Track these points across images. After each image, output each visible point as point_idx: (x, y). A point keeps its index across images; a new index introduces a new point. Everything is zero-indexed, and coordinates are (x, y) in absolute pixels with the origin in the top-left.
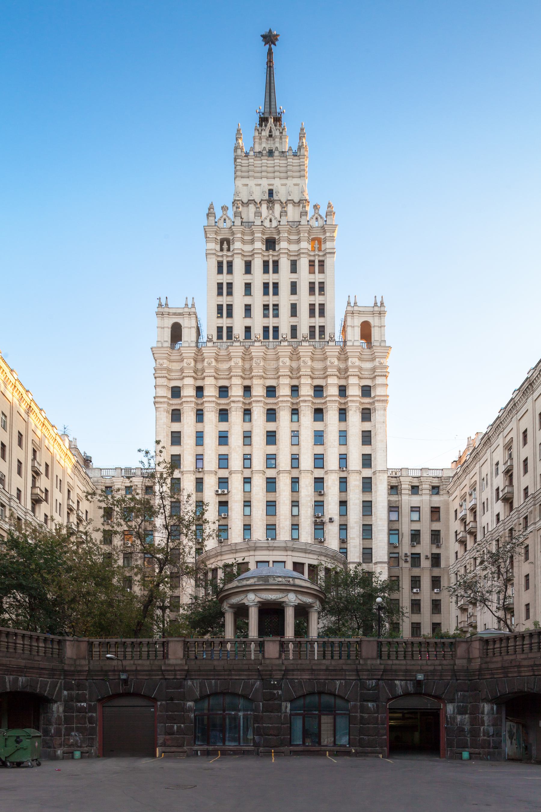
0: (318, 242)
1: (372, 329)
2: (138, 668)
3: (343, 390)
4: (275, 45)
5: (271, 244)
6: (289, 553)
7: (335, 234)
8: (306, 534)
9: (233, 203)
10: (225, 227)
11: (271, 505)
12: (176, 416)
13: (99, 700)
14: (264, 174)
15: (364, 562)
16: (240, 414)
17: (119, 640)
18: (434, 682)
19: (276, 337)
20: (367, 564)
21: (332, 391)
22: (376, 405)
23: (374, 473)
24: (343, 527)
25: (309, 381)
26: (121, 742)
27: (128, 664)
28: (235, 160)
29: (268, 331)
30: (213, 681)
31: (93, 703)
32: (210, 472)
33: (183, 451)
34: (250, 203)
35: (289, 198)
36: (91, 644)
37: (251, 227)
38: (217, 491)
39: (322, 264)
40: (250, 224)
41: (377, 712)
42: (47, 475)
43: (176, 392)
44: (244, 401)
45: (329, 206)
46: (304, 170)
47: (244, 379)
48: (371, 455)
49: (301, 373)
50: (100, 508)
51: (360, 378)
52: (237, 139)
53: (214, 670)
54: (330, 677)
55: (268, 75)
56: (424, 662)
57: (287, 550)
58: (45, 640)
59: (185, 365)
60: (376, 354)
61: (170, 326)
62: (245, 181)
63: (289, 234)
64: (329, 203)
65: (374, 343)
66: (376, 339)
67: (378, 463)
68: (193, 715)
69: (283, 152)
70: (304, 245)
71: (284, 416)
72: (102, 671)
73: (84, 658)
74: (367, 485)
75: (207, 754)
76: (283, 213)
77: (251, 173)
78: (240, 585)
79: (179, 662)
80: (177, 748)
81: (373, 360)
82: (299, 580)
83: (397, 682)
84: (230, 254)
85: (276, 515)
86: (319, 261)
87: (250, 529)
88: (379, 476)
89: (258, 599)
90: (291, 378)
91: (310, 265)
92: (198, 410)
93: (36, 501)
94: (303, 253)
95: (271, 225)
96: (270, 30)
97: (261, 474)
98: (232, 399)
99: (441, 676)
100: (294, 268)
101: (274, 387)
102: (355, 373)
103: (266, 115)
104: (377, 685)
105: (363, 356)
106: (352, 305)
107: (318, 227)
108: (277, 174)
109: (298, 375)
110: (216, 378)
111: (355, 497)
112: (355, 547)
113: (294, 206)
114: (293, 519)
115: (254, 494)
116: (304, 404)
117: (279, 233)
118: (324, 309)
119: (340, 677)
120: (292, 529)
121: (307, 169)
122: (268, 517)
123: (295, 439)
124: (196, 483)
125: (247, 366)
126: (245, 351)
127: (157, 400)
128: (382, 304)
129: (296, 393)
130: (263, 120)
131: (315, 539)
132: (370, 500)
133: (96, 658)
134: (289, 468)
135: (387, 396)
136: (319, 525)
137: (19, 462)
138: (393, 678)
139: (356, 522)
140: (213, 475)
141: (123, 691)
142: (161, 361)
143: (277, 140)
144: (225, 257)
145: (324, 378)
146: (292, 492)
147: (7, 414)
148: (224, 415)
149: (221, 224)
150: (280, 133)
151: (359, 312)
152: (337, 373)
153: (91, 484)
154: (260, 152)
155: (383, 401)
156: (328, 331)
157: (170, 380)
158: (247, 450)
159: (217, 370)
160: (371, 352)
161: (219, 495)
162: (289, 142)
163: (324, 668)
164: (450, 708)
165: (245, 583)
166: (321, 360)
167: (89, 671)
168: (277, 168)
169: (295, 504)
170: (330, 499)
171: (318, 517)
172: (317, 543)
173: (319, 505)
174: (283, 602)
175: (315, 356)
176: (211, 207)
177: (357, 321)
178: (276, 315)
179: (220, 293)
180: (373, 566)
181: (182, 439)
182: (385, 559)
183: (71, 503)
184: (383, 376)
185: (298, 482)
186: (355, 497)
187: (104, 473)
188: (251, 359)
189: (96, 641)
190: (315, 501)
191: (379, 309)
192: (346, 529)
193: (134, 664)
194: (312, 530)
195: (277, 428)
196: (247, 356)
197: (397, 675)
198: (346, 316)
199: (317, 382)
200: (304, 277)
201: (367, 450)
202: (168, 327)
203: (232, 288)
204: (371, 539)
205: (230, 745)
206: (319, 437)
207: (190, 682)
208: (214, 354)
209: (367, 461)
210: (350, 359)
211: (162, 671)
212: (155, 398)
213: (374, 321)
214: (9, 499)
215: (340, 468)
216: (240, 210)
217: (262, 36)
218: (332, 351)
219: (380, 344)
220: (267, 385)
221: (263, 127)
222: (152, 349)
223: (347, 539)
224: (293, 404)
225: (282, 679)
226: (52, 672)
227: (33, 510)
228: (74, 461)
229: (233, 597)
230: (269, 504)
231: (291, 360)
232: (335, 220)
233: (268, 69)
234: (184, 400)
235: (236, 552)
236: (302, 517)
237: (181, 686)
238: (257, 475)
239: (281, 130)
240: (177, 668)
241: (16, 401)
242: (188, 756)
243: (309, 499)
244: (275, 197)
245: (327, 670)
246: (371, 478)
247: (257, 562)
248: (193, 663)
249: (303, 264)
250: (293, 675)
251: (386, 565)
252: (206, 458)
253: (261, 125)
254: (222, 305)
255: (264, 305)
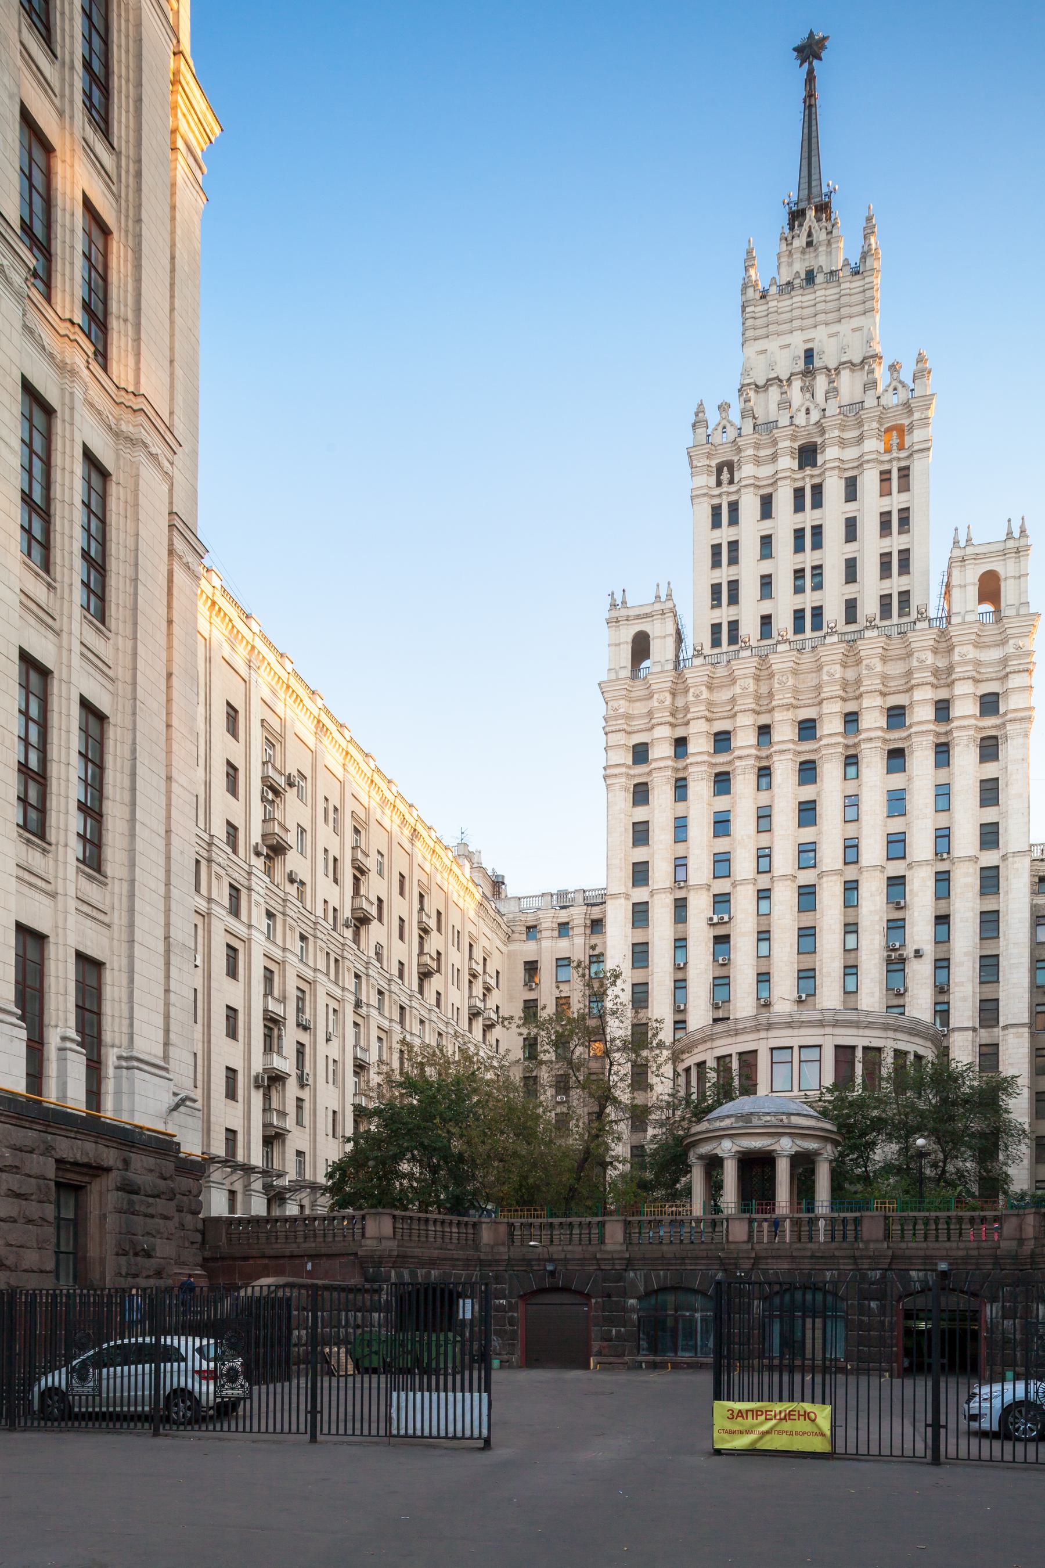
0: (897, 433)
1: (1003, 584)
2: (568, 1256)
3: (943, 709)
4: (820, 59)
5: (808, 455)
6: (828, 1030)
7: (931, 413)
8: (872, 995)
9: (739, 391)
10: (724, 440)
11: (807, 934)
12: (641, 794)
13: (521, 1297)
14: (797, 323)
15: (981, 1026)
16: (752, 778)
17: (544, 1220)
18: (968, 1273)
19: (817, 626)
20: (989, 1030)
21: (922, 714)
22: (1008, 728)
23: (1004, 858)
24: (942, 964)
25: (878, 701)
26: (554, 1349)
27: (555, 1250)
28: (744, 308)
29: (803, 617)
30: (662, 1273)
31: (513, 1301)
32: (699, 887)
33: (653, 855)
34: (771, 385)
35: (843, 360)
36: (511, 1226)
37: (771, 431)
38: (711, 919)
39: (905, 473)
40: (771, 426)
41: (884, 1314)
42: (439, 930)
43: (640, 753)
44: (759, 754)
45: (921, 359)
46: (873, 298)
47: (758, 713)
48: (998, 823)
49: (862, 689)
50: (521, 1034)
51: (976, 681)
52: (746, 269)
53: (663, 1258)
54: (817, 1267)
55: (806, 125)
56: (954, 1245)
57: (824, 1026)
58: (459, 1224)
59: (656, 704)
60: (1009, 632)
61: (630, 639)
62: (761, 345)
63: (843, 431)
64: (920, 354)
65: (1006, 612)
66: (1009, 603)
67: (1011, 839)
68: (635, 1317)
69: (832, 272)
70: (872, 445)
71: (831, 771)
72: (524, 1260)
73: (503, 1244)
74: (990, 880)
75: (654, 1366)
76: (833, 392)
77: (772, 328)
78: (711, 1127)
79: (618, 1248)
80: (616, 1357)
81: (1004, 642)
82: (797, 1118)
83: (913, 1273)
84: (733, 488)
85: (815, 952)
86: (900, 469)
87: (769, 981)
88: (1014, 863)
89: (736, 1148)
90: (844, 700)
91: (882, 481)
92: (677, 780)
93: (425, 975)
94: (868, 461)
95: (808, 419)
96: (811, 34)
97: (789, 882)
98: (737, 753)
99: (977, 1264)
100: (851, 491)
101: (814, 721)
102: (966, 675)
103: (802, 205)
104: (883, 1276)
105: (983, 639)
106: (962, 544)
107: (897, 406)
108: (821, 317)
109: (858, 693)
110: (708, 720)
111: (966, 906)
112: (964, 999)
113: (852, 371)
114: (848, 956)
115: (776, 917)
116: (869, 745)
117: (823, 432)
118: (908, 559)
119: (832, 1267)
120: (845, 975)
121: (878, 295)
122: (801, 956)
123: (851, 813)
124: (676, 907)
125: (764, 690)
126: (759, 664)
127: (609, 772)
128: (1023, 531)
129: (853, 726)
130: (796, 216)
131: (888, 989)
132: (996, 909)
133: (517, 1243)
134: (839, 864)
135: (1031, 708)
136: (896, 963)
137: (401, 920)
138: (907, 1267)
139: (966, 954)
140: (704, 892)
141: (552, 1285)
142: (615, 704)
143: (822, 249)
144: (724, 497)
145: (907, 691)
146: (845, 907)
147: (385, 852)
148: (722, 782)
149: (718, 438)
150: (828, 234)
151: (976, 557)
152: (932, 679)
153: (504, 926)
154: (789, 283)
155: (1022, 719)
156: (915, 601)
157: (630, 733)
158: (764, 840)
159: (710, 704)
160: (999, 628)
161: (714, 924)
162: (845, 250)
163: (809, 1254)
164: (991, 1311)
165: (718, 1124)
166: (900, 659)
167: (509, 1260)
168: (820, 307)
169: (851, 928)
170: (916, 914)
171: (894, 950)
172: (891, 997)
173: (896, 926)
174: (773, 1151)
175: (890, 653)
176: (700, 410)
177: (972, 575)
178: (818, 586)
179: (716, 563)
180: (1001, 1033)
181: (650, 834)
182: (1025, 1018)
183: (474, 966)
184: (1024, 671)
185: (857, 889)
186: (966, 906)
187: (524, 904)
188: (771, 676)
189: (517, 1222)
190: (888, 921)
191: (1016, 545)
192: (948, 967)
193: (563, 1251)
194: (881, 974)
195: (818, 794)
196: (764, 672)
197: (911, 1264)
198: (950, 568)
199: (894, 701)
200: (871, 503)
201: (990, 815)
202: (627, 643)
203: (737, 550)
204: (998, 982)
205: (685, 1356)
206: (897, 803)
207: (632, 1274)
208: (706, 678)
209: (990, 835)
210: (957, 650)
211: (598, 1260)
212: (605, 769)
213: (1005, 569)
214: (389, 980)
215: (936, 854)
216: (752, 403)
217: (795, 49)
218: (922, 638)
219: (1018, 610)
220: (800, 718)
221: (796, 231)
222: (599, 684)
223: (948, 985)
224: (847, 747)
225: (752, 1269)
226: (467, 1263)
227: (421, 991)
228: (478, 897)
229: (702, 1144)
230: (802, 932)
231: (845, 667)
232: (931, 385)
233: (807, 112)
234: (654, 765)
235: (736, 1035)
236: (864, 952)
237: (620, 1279)
238: (780, 884)
239: (829, 228)
240: (616, 1256)
241: (395, 829)
242: (629, 1369)
243: (877, 918)
244: (818, 363)
245: (812, 1257)
246: (998, 867)
247: (772, 1049)
248: (636, 1248)
249: (869, 482)
250: (767, 1264)
251: (1026, 1030)
252: (692, 863)
253: (792, 229)
254: (720, 584)
255: (796, 571)
